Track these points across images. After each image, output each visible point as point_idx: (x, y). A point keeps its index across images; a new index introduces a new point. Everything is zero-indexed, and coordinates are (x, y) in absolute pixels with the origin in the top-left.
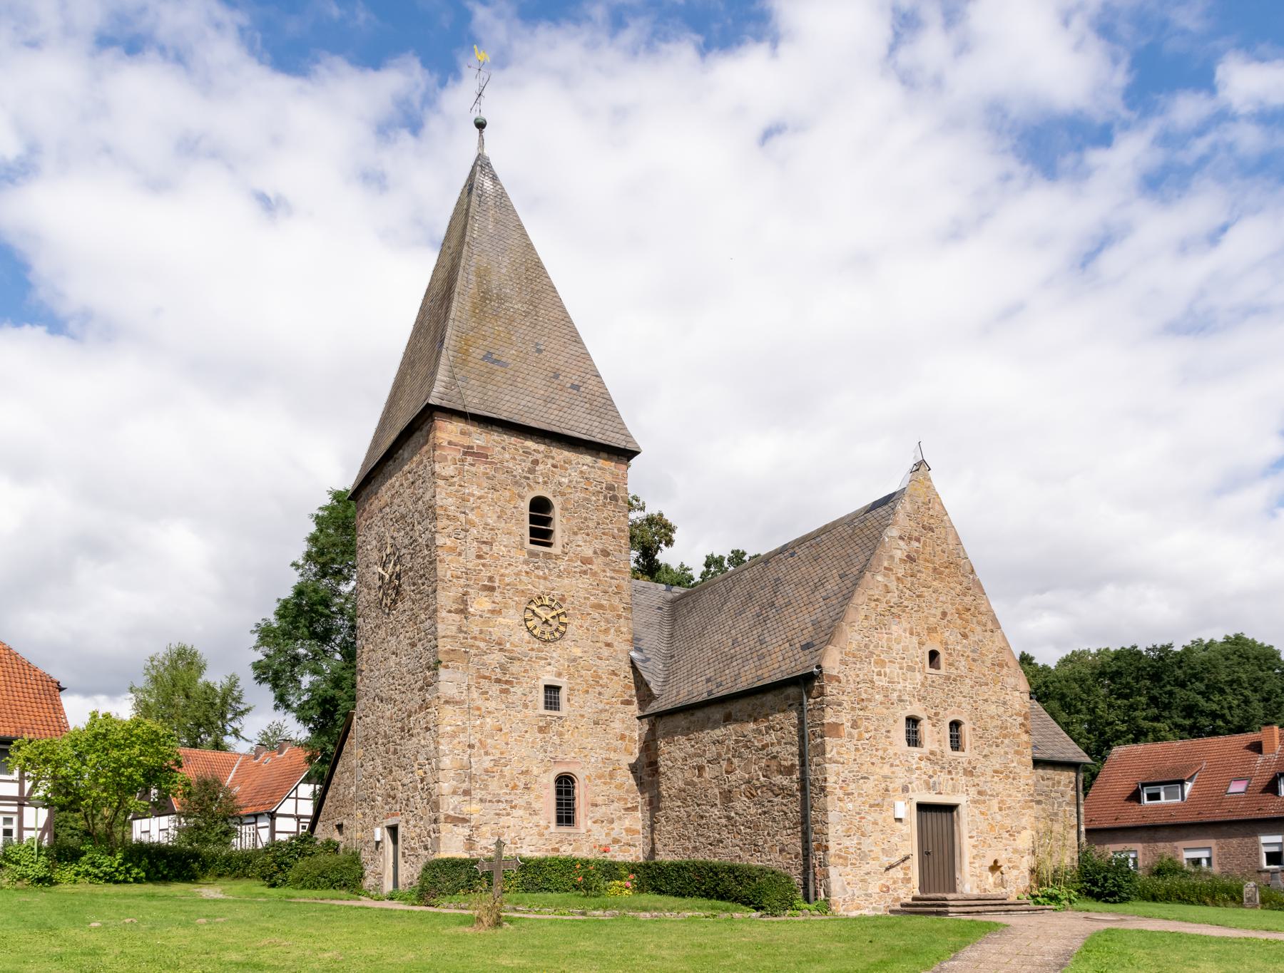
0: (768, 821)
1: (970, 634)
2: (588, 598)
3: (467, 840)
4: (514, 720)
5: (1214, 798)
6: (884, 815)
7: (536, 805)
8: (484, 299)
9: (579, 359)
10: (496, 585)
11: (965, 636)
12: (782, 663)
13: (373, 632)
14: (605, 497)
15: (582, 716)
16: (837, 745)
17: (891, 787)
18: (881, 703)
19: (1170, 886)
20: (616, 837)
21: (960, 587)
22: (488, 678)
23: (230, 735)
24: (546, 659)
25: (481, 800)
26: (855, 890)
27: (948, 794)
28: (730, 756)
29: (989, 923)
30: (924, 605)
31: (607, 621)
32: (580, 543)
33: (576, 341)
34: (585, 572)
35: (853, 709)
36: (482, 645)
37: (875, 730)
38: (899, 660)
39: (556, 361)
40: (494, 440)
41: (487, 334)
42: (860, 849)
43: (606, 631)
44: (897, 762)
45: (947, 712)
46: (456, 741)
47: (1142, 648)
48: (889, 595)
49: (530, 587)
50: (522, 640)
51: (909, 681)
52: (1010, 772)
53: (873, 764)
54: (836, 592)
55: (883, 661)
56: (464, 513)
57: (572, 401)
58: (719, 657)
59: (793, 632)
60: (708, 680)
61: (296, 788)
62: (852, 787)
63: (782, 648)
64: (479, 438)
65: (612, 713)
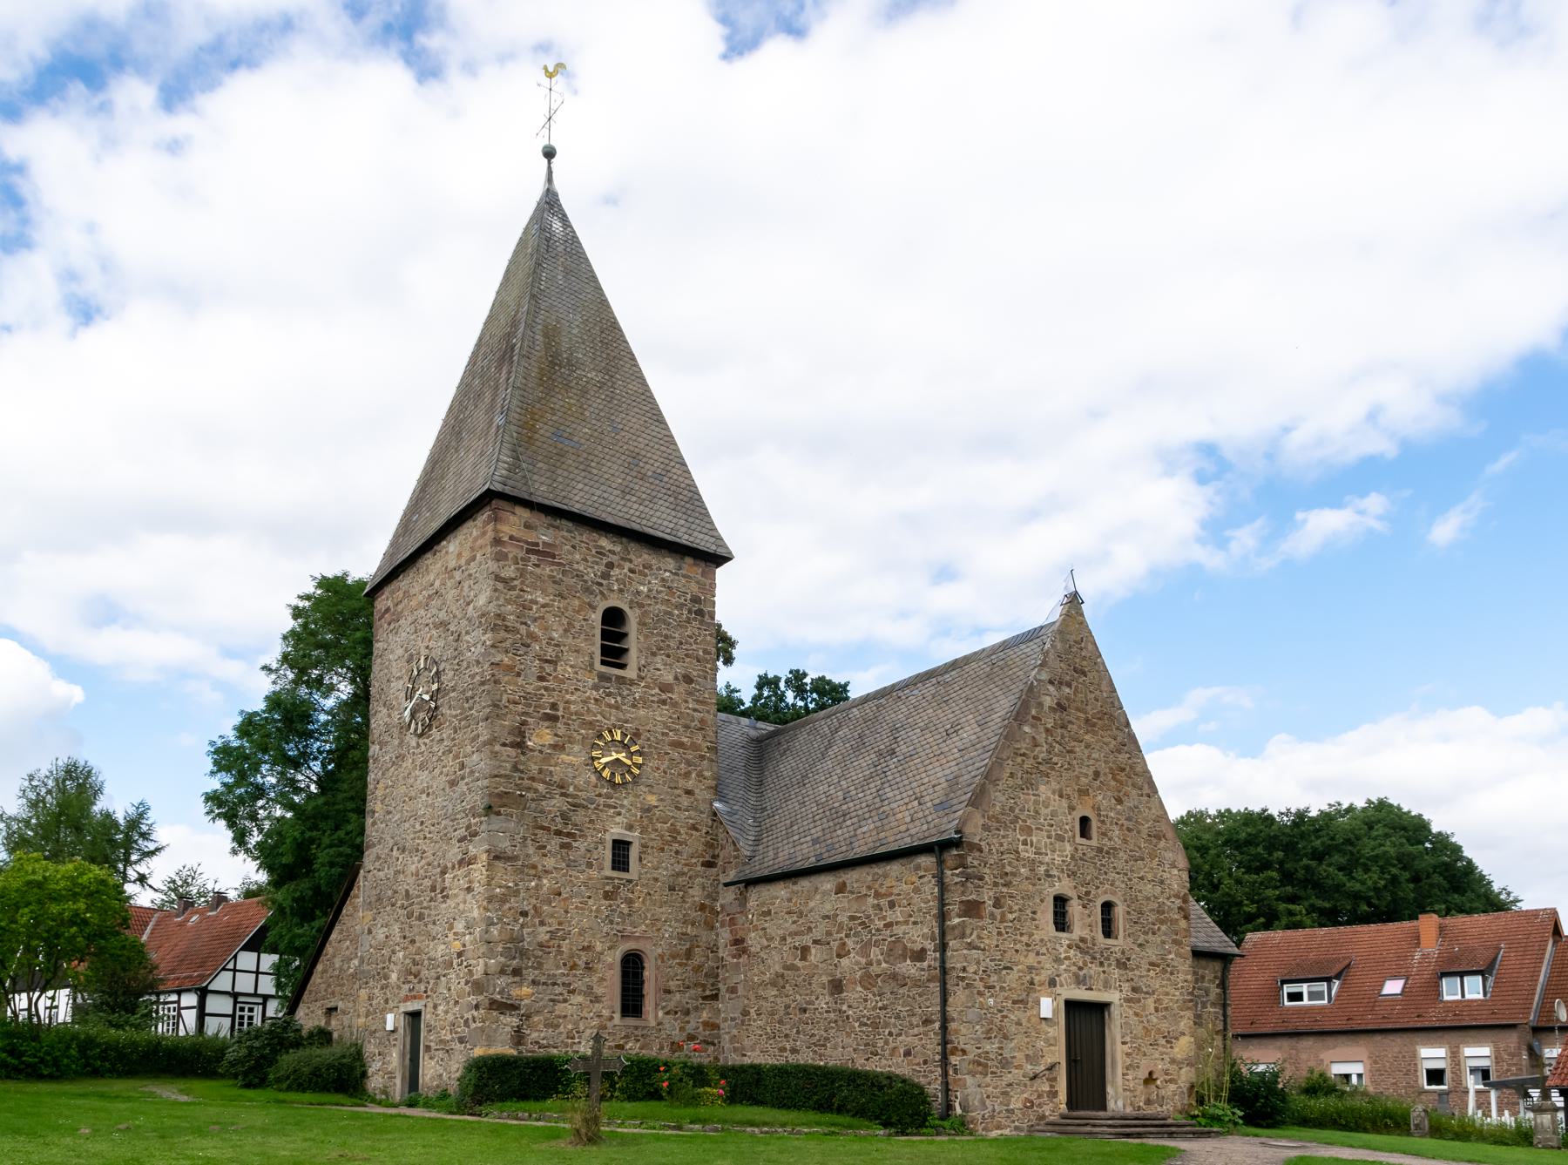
0: (890, 1018)
2: (667, 734)
3: (515, 1031)
4: (575, 881)
5: (1366, 1000)
7: (599, 990)
8: (553, 364)
9: (662, 442)
10: (560, 713)
11: (1119, 801)
12: (911, 826)
14: (690, 612)
15: (656, 880)
16: (977, 927)
17: (1037, 979)
18: (1027, 878)
19: (1325, 1108)
21: (1114, 742)
22: (547, 829)
23: (134, 882)
24: (616, 808)
25: (534, 982)
26: (996, 1105)
27: (1100, 990)
28: (843, 935)
29: (1173, 1149)
30: (1075, 762)
31: (688, 763)
32: (659, 666)
33: (658, 421)
34: (664, 702)
36: (541, 787)
39: (635, 444)
40: (563, 537)
41: (557, 407)
43: (687, 775)
44: (1044, 950)
45: (1099, 891)
46: (507, 906)
47: (1274, 811)
48: (1038, 749)
49: (599, 717)
50: (587, 782)
52: (1168, 966)
53: (1017, 951)
54: (974, 742)
56: (525, 624)
57: (654, 493)
58: (828, 813)
59: (922, 788)
61: (235, 957)
63: (909, 807)
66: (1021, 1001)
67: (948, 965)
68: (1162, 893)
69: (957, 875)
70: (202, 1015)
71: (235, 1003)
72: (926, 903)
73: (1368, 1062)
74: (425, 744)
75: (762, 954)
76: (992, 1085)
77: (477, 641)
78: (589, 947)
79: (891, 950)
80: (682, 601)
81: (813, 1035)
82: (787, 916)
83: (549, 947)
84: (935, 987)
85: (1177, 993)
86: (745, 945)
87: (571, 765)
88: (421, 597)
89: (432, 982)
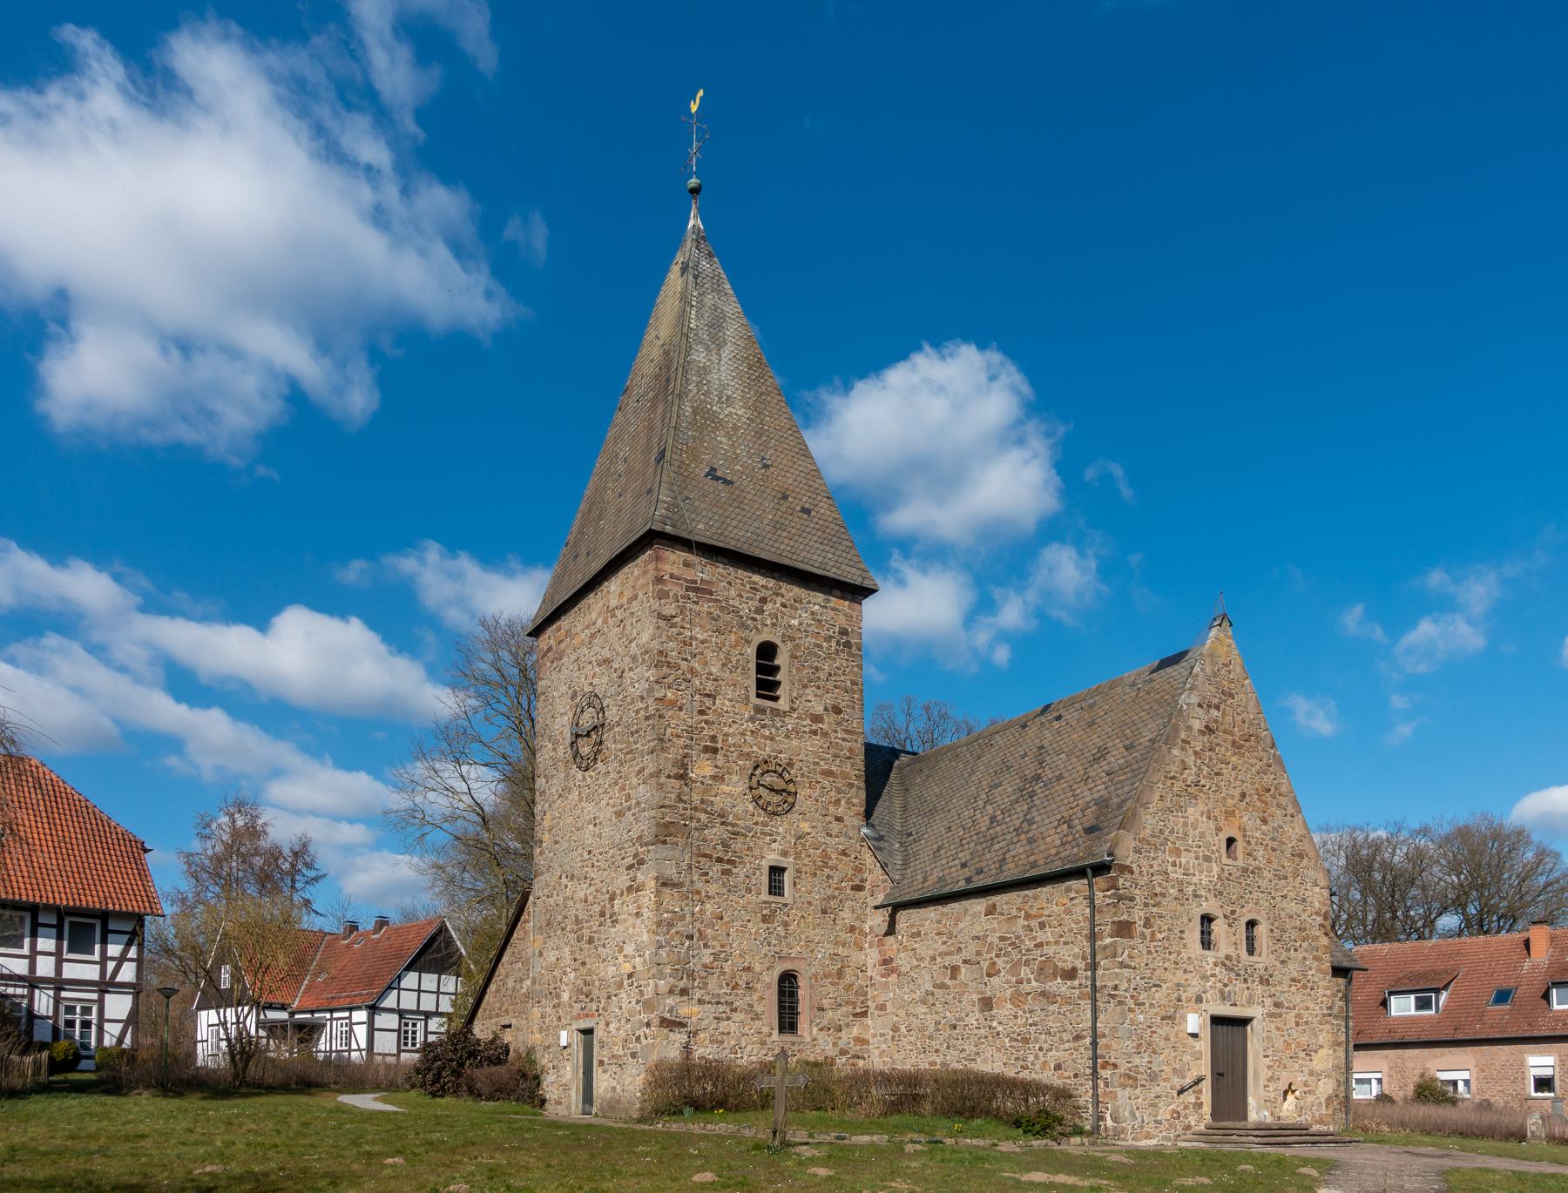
1: (1269, 819)
2: (818, 764)
6: (1176, 1029)
7: (758, 1008)
9: (809, 476)
10: (719, 746)
13: (560, 796)
14: (838, 644)
15: (810, 903)
18: (1176, 899)
20: (844, 1047)
26: (1145, 1116)
28: (993, 955)
31: (839, 791)
32: (809, 698)
34: (815, 733)
35: (1146, 905)
37: (1169, 930)
38: (1195, 849)
40: (719, 574)
42: (1150, 1068)
43: (838, 802)
44: (1191, 968)
45: (1244, 910)
48: (1187, 771)
49: (755, 748)
51: (1205, 873)
53: (1166, 969)
55: (1178, 850)
57: (803, 528)
60: (964, 865)
62: (1143, 997)
63: (1059, 830)
64: (705, 571)
65: (841, 901)
66: (1169, 1017)
67: (1098, 984)
68: (1304, 911)
69: (1109, 897)
70: (371, 1030)
71: (401, 1017)
72: (1077, 924)
73: (1474, 1071)
74: (591, 777)
75: (912, 974)
76: (1141, 1097)
77: (641, 677)
78: (749, 968)
79: (1042, 969)
80: (831, 633)
81: (963, 1050)
82: (936, 937)
83: (713, 968)
84: (1086, 1004)
85: (1317, 1008)
86: (894, 964)
87: (729, 795)
88: (583, 636)
89: (603, 1001)
